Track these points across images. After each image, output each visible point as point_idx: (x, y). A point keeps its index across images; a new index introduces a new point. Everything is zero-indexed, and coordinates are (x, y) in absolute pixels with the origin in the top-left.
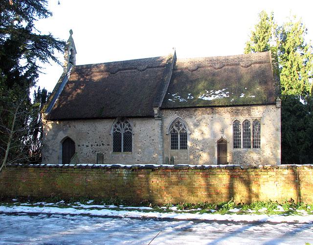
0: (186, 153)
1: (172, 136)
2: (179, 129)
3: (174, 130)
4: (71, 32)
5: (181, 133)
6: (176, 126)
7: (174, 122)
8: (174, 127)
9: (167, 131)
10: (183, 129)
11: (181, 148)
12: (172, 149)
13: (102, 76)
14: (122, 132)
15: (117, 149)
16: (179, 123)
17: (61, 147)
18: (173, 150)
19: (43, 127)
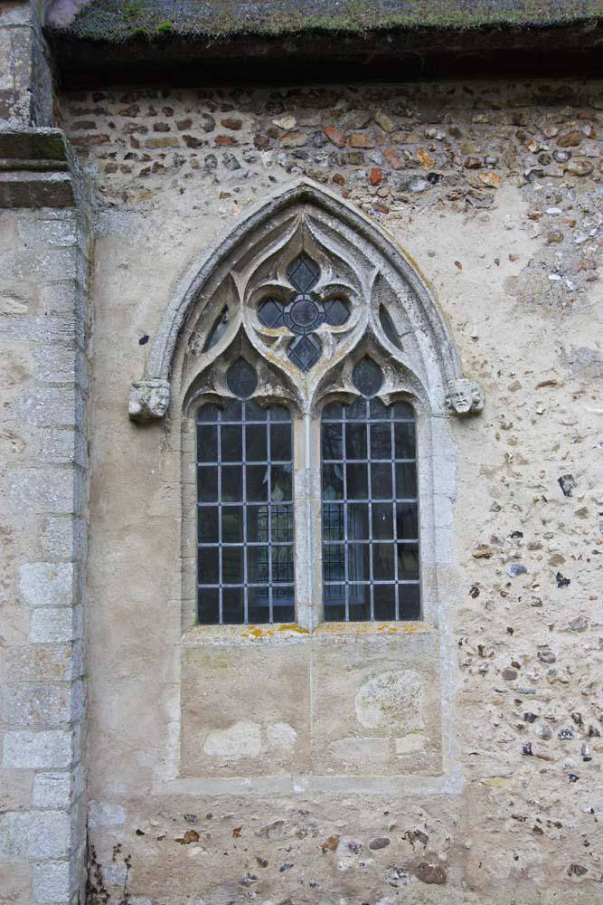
0: (409, 678)
1: (205, 436)
2: (305, 353)
3: (241, 358)
5: (331, 404)
6: (270, 302)
7: (235, 253)
8: (247, 319)
9: (140, 369)
10: (369, 361)
11: (332, 612)
12: (207, 615)
13: (276, 122)
15: (236, 582)
16: (304, 263)
18: (219, 635)
19: (51, 194)
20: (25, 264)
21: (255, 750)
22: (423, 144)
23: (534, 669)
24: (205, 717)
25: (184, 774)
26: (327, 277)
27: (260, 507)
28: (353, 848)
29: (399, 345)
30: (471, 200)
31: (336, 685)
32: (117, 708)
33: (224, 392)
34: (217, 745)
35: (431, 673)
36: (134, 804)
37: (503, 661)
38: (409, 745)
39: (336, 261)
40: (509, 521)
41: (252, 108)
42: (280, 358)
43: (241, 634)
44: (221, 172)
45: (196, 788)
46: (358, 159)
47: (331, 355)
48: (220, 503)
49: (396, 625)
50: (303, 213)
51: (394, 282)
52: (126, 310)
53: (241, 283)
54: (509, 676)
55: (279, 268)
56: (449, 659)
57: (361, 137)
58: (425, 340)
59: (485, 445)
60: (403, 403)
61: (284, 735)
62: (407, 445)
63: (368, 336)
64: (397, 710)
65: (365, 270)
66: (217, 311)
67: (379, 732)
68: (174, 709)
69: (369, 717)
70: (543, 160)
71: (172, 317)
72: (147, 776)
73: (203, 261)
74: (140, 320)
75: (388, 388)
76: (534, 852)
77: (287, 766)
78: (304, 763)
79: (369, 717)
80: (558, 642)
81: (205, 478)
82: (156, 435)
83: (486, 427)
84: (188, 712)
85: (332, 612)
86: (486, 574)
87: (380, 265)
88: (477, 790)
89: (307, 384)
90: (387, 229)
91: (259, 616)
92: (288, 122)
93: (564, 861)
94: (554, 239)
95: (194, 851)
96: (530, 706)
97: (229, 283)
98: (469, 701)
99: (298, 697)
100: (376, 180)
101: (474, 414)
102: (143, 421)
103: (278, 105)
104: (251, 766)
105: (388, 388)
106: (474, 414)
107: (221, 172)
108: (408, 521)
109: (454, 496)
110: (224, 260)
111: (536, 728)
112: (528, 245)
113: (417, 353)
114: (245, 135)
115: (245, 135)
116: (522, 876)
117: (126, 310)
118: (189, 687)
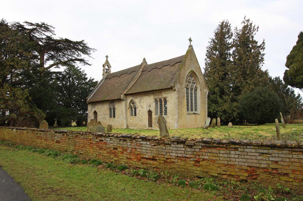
4: (107, 57)
8: (132, 104)
14: (112, 107)
15: (111, 117)
17: (94, 115)
30: (137, 99)
55: (132, 102)
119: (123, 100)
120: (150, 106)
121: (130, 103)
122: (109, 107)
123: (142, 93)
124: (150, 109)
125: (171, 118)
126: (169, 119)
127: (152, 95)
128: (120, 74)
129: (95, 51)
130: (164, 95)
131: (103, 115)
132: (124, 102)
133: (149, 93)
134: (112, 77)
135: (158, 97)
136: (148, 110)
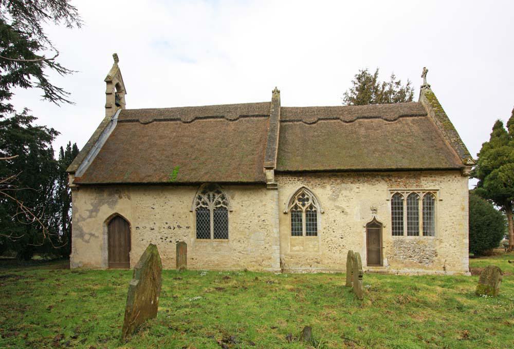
1: (292, 215)
2: (304, 205)
3: (296, 207)
5: (307, 211)
6: (299, 200)
7: (295, 194)
8: (297, 201)
10: (311, 207)
11: (307, 234)
12: (292, 235)
15: (296, 232)
16: (303, 195)
17: (106, 229)
18: (294, 237)
20: (273, 196)
21: (298, 249)
22: (318, 181)
23: (330, 241)
24: (292, 245)
25: (291, 251)
26: (306, 196)
27: (12, 156)
28: (309, 260)
29: (315, 204)
30: (324, 187)
31: (307, 243)
32: (283, 245)
33: (294, 210)
34: (294, 248)
35: (318, 242)
36: (285, 254)
37: (327, 240)
38: (315, 249)
39: (307, 195)
40: (328, 225)
41: (297, 176)
42: (301, 206)
43: (297, 237)
44: (294, 184)
45: (292, 253)
46: (310, 182)
47: (307, 206)
48: (394, 231)
49: (315, 236)
50: (303, 189)
51: (314, 197)
52: (283, 200)
53: (296, 197)
54: (327, 242)
55: (301, 196)
56: (320, 240)
57: (310, 180)
58: (318, 204)
59: (325, 216)
60: (315, 211)
61: (302, 248)
62: (316, 216)
63: (311, 204)
64: (314, 246)
65: (310, 196)
66: (319, 277)
67: (312, 248)
68: (289, 244)
69: (311, 246)
70: (333, 182)
71: (289, 201)
72: (287, 252)
73: (291, 196)
74: (284, 202)
75: (314, 209)
76: (330, 261)
77: (302, 251)
78: (304, 251)
79: (311, 246)
80: (333, 239)
81: (292, 220)
82: (286, 215)
83: (325, 214)
84: (291, 245)
85: (307, 234)
86: (325, 231)
87: (313, 195)
88: (323, 254)
89: (304, 209)
90: (313, 191)
91: (298, 235)
92: (301, 178)
93: (333, 262)
94: (334, 192)
95: (292, 259)
96: (330, 245)
97: (295, 197)
98: (323, 245)
99: (303, 244)
100: (312, 185)
101: (323, 213)
102: (285, 213)
103: (300, 176)
104: (297, 251)
105: (314, 209)
106: (323, 213)
107: (294, 184)
108: (316, 225)
109: (321, 221)
110: (294, 194)
111: (330, 248)
112: (331, 193)
113: (317, 205)
114: (296, 180)
115: (296, 180)
116: (328, 263)
117: (283, 200)
118: (291, 242)
119: (274, 187)
120: (374, 210)
121: (292, 200)
122: (195, 207)
123: (352, 174)
124: (375, 219)
125: (451, 242)
126: (443, 245)
127: (383, 182)
128: (239, 114)
129: (74, 24)
130: (427, 184)
131: (166, 231)
132: (272, 194)
133: (374, 176)
134: (155, 120)
135: (406, 187)
136: (369, 219)
